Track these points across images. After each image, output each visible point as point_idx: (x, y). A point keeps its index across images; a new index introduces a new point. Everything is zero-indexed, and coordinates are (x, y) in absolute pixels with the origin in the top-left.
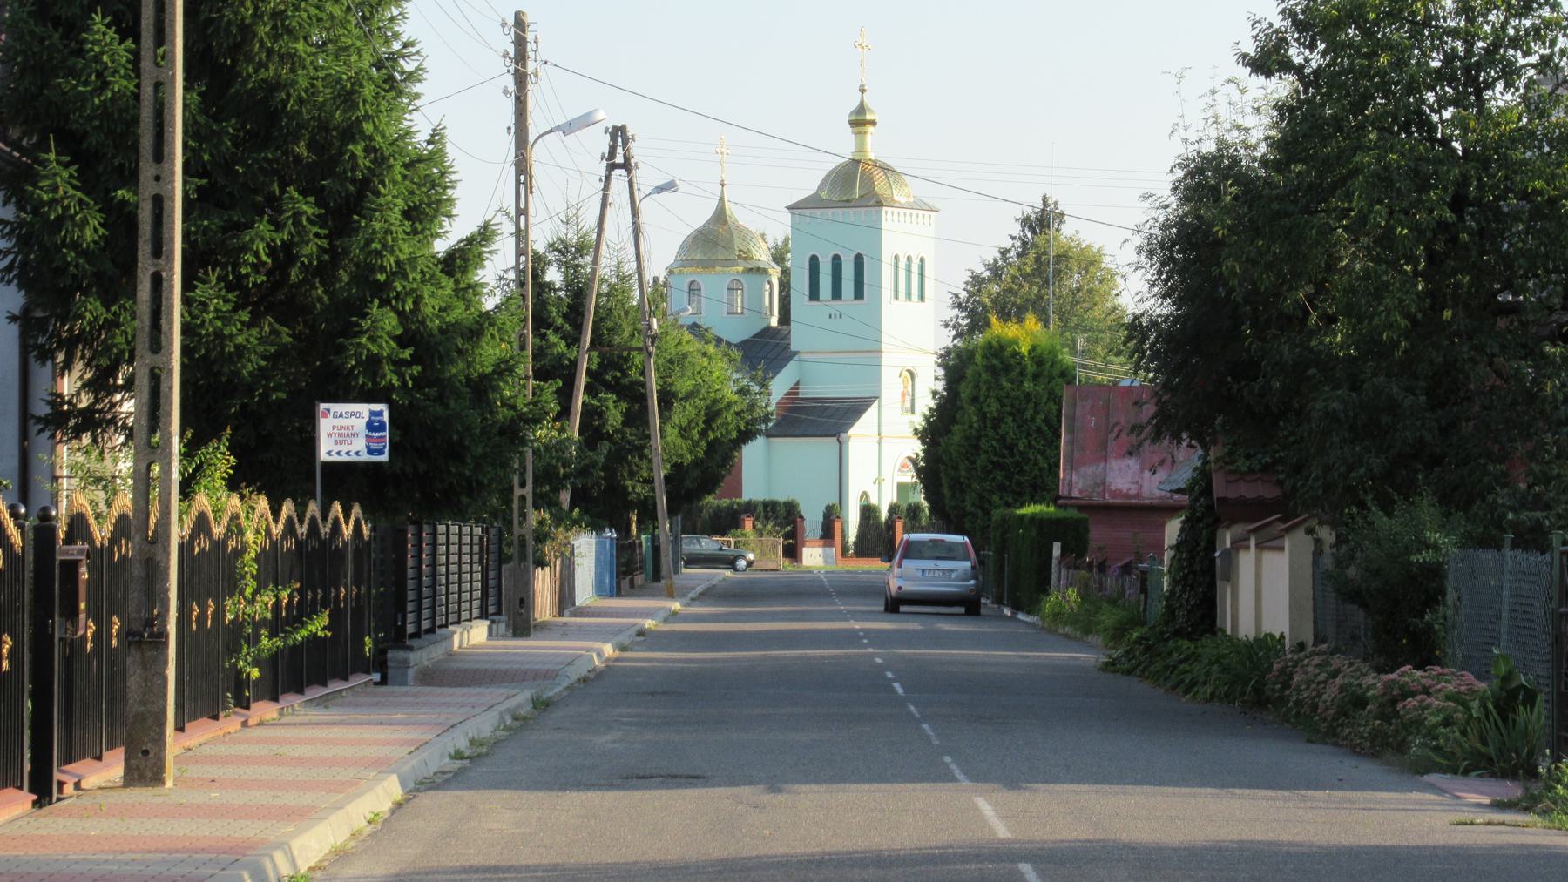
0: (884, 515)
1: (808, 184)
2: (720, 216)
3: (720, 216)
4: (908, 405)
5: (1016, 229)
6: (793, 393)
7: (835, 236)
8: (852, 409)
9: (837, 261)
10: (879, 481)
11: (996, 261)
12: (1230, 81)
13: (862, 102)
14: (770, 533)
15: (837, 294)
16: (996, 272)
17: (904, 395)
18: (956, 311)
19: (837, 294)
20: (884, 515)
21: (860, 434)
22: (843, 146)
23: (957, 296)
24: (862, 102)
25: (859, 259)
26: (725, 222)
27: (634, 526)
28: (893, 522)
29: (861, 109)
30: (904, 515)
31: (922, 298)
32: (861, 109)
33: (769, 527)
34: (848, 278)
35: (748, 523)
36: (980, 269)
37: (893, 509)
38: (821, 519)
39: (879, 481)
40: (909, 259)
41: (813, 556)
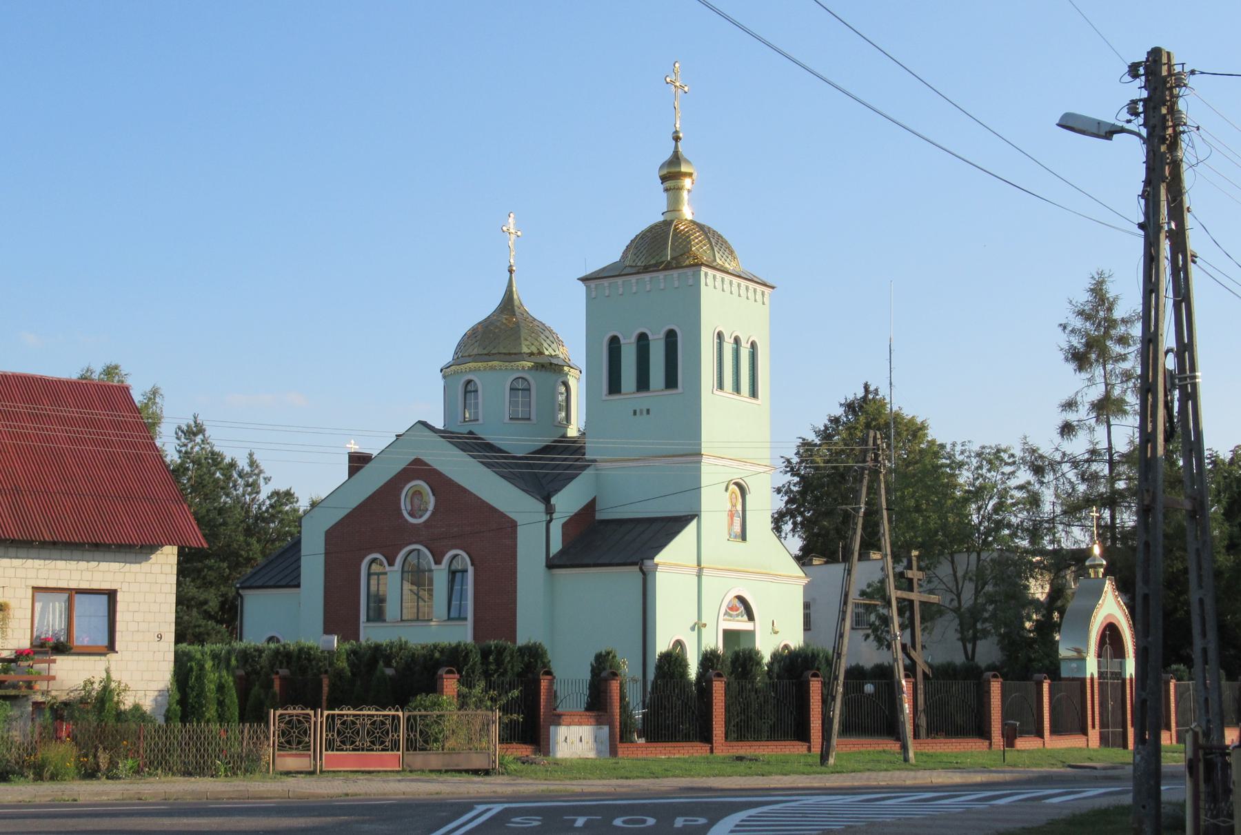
0: (693, 672)
1: (611, 253)
2: (508, 304)
3: (508, 304)
4: (737, 528)
5: (839, 412)
6: (591, 507)
7: (643, 310)
8: (665, 528)
9: (643, 340)
10: (699, 627)
11: (826, 428)
12: (776, 633)
13: (676, 153)
14: (479, 704)
15: (643, 383)
16: (826, 435)
17: (731, 515)
18: (788, 477)
19: (643, 383)
20: (693, 672)
21: (673, 560)
22: (651, 212)
23: (789, 461)
24: (676, 153)
25: (671, 336)
26: (513, 313)
27: (325, 689)
28: (710, 682)
29: (676, 159)
30: (727, 669)
31: (754, 393)
32: (676, 159)
33: (477, 690)
34: (650, 363)
35: (451, 685)
36: (812, 437)
37: (708, 660)
38: (587, 676)
39: (699, 627)
40: (737, 341)
41: (575, 740)
